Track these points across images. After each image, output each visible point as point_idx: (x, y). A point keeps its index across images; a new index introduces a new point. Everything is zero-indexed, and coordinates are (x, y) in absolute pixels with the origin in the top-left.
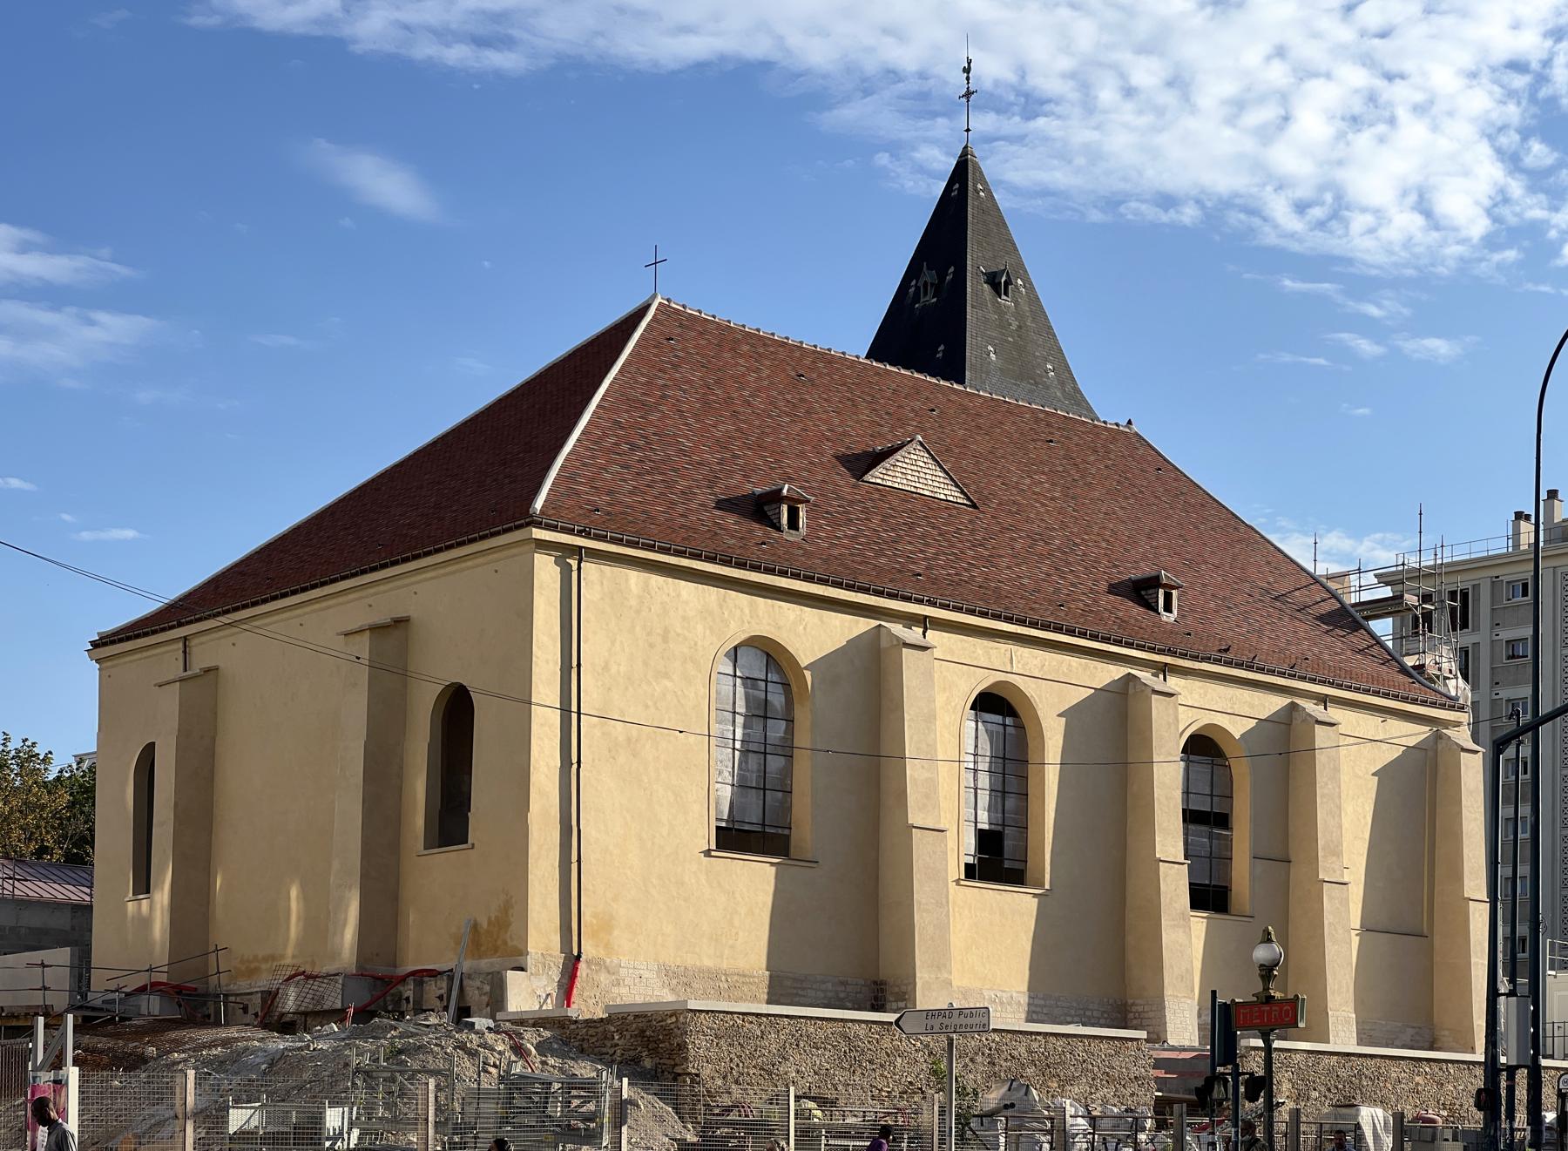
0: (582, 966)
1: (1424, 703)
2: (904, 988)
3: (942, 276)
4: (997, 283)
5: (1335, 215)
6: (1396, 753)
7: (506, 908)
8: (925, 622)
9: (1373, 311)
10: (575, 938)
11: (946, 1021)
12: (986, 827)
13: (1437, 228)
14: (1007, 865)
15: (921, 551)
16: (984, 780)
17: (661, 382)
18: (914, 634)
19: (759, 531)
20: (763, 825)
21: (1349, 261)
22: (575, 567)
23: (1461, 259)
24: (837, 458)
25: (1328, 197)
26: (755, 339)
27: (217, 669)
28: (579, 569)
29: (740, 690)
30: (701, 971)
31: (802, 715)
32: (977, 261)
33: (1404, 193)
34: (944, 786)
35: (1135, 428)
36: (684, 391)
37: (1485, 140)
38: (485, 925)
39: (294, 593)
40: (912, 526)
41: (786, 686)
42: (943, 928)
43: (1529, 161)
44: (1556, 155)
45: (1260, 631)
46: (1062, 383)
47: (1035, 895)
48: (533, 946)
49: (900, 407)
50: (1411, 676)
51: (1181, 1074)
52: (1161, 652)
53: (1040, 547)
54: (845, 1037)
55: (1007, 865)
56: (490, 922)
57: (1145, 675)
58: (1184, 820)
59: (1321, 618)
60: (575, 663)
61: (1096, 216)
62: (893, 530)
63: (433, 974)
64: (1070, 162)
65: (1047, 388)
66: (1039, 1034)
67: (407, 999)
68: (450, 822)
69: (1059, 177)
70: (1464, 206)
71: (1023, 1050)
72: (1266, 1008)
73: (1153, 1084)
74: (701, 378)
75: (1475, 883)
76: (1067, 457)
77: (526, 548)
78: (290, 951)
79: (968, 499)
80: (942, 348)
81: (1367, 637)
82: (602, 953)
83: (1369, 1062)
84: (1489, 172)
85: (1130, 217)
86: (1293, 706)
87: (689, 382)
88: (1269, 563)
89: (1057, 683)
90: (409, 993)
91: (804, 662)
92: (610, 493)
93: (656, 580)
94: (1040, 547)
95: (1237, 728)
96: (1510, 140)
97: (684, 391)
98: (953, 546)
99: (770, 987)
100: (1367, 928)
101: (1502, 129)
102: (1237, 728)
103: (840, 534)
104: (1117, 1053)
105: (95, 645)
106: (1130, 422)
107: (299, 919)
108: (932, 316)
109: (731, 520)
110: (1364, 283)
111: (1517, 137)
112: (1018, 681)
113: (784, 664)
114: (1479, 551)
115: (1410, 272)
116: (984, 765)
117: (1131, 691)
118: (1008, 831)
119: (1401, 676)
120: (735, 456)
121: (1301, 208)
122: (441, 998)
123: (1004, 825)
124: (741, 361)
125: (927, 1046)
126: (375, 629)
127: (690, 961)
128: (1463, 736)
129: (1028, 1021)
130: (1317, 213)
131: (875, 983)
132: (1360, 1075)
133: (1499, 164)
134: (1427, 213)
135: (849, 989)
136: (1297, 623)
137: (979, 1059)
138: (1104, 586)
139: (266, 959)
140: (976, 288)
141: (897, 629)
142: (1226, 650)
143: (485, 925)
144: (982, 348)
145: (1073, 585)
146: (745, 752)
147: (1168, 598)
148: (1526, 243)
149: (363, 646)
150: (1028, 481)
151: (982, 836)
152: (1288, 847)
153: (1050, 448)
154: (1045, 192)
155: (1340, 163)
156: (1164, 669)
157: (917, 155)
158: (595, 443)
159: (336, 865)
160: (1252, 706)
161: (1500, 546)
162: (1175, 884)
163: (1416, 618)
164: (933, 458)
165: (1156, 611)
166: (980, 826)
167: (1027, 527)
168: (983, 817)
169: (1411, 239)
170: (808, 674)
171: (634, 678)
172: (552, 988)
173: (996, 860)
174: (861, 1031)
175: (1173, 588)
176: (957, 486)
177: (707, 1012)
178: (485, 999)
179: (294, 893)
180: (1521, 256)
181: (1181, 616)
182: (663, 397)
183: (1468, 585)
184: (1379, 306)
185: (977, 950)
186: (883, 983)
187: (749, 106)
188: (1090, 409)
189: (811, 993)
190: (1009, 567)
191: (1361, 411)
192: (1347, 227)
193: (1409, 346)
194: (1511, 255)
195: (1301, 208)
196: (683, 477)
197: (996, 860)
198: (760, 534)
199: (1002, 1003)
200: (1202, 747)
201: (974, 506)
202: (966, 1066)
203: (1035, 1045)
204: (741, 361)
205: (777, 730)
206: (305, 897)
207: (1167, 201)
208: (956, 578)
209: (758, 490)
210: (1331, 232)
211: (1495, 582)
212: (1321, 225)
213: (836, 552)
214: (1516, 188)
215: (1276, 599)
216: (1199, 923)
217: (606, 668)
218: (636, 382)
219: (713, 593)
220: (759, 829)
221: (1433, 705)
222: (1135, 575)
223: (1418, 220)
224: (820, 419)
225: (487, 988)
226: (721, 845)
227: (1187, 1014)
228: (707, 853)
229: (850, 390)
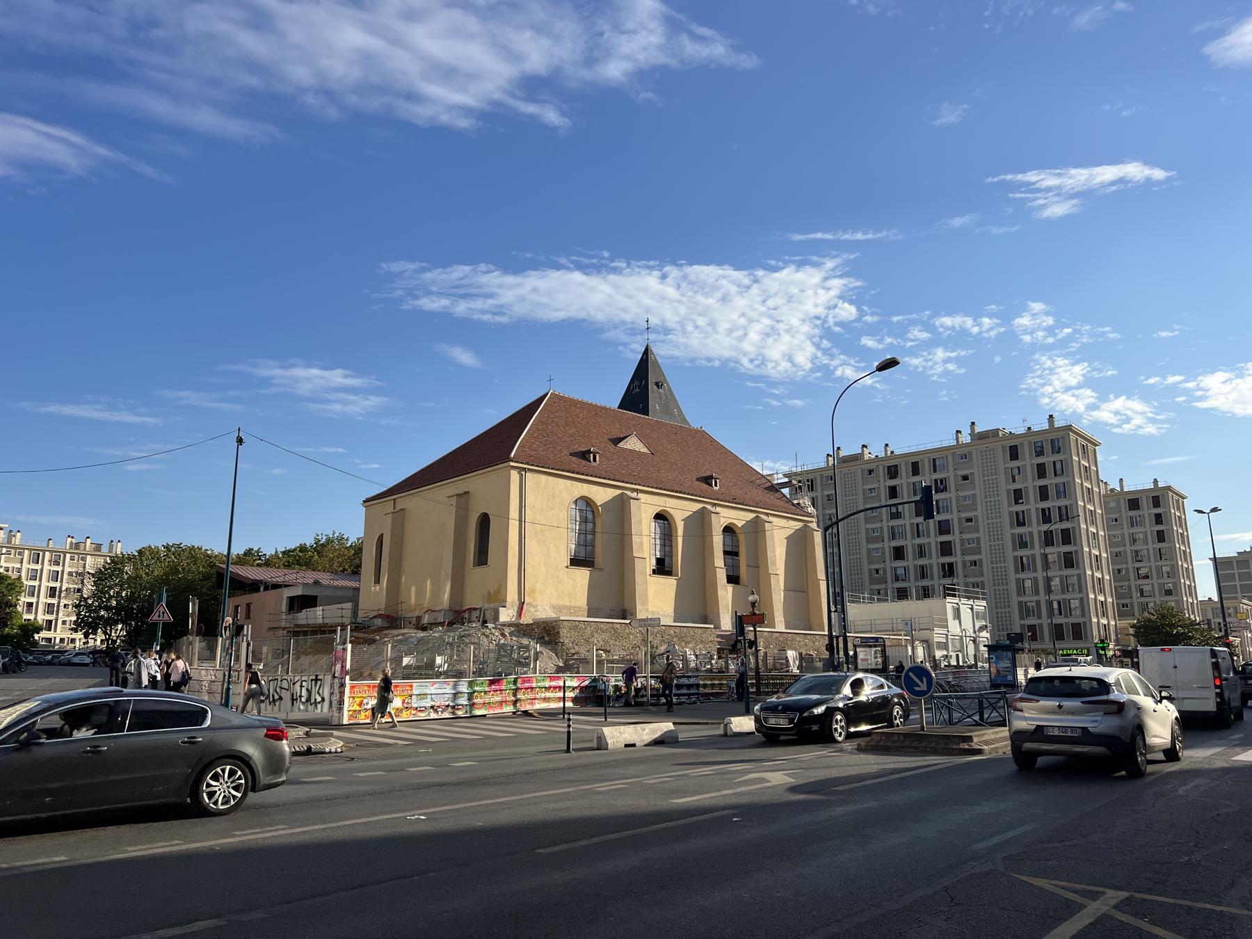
7: (500, 586)
16: (658, 542)
18: (634, 495)
19: (584, 462)
32: (652, 379)
42: (646, 591)
48: (509, 599)
57: (709, 507)
61: (688, 364)
68: (482, 557)
69: (676, 353)
70: (803, 359)
84: (810, 349)
89: (681, 510)
95: (740, 524)
96: (816, 340)
100: (786, 589)
102: (740, 524)
110: (773, 384)
112: (735, 522)
121: (751, 361)
128: (814, 526)
140: (651, 386)
141: (628, 493)
144: (654, 404)
151: (658, 560)
162: (721, 575)
171: (542, 511)
173: (663, 568)
197: (663, 568)
206: (432, 583)
207: (710, 360)
212: (758, 366)
214: (819, 354)
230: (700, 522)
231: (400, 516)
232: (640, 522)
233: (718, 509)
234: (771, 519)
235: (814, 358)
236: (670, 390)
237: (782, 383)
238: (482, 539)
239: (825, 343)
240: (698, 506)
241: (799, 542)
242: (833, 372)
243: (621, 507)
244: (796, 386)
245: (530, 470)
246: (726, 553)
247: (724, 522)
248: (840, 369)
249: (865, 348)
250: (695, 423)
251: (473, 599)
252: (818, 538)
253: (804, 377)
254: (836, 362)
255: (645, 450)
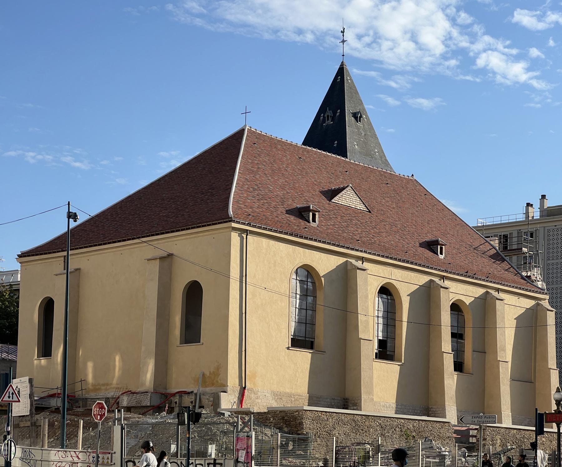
0: (246, 391)
1: (533, 291)
2: (356, 401)
3: (335, 113)
4: (357, 117)
5: (374, 42)
6: (523, 311)
7: (218, 368)
8: (363, 259)
9: (393, 84)
10: (244, 380)
11: (480, 420)
12: (381, 338)
13: (421, 49)
14: (388, 353)
15: (357, 231)
16: (381, 320)
17: (256, 162)
18: (359, 264)
19: (303, 223)
20: (306, 337)
21: (381, 62)
22: (245, 237)
23: (432, 63)
24: (320, 192)
25: (371, 33)
26: (280, 142)
27: (79, 269)
28: (247, 238)
29: (298, 284)
30: (285, 393)
31: (320, 295)
32: (349, 108)
33: (405, 32)
34: (370, 325)
35: (415, 177)
36: (264, 165)
37: (440, 10)
38: (208, 374)
39: (119, 241)
40: (351, 220)
41: (313, 283)
42: (371, 378)
43: (459, 21)
44: (472, 18)
45: (472, 262)
46: (381, 157)
47: (399, 365)
48: (229, 383)
49: (335, 170)
50: (526, 280)
51: (462, 436)
52: (442, 271)
53: (394, 228)
54: (354, 420)
55: (388, 353)
56: (210, 373)
57: (436, 280)
58: (452, 337)
59: (490, 257)
60: (244, 275)
61: (267, 36)
62: (346, 222)
63: (188, 393)
64: (255, 12)
65: (376, 159)
66: (417, 420)
67: (176, 403)
68: (191, 333)
69: (251, 19)
70: (433, 38)
71: (411, 426)
72: (558, 415)
73: (454, 439)
74: (269, 160)
75: (552, 362)
76: (394, 190)
77: (228, 230)
78: (115, 382)
79: (368, 209)
80: (336, 142)
81: (508, 264)
82: (252, 386)
83: (527, 432)
84: (443, 24)
85: (283, 37)
86: (487, 292)
87: (265, 161)
88: (469, 234)
89: (407, 283)
90: (177, 400)
91: (322, 274)
92: (251, 208)
93: (272, 242)
94: (394, 228)
95: (468, 301)
96: (452, 11)
97: (264, 165)
98: (366, 228)
99: (309, 400)
100: (513, 379)
101: (448, 6)
102: (468, 301)
103: (329, 224)
104: (442, 427)
105: (20, 256)
106: (413, 175)
107: (119, 369)
108: (331, 128)
109: (292, 218)
110: (389, 74)
111: (454, 10)
112: (394, 282)
113: (314, 275)
114: (512, 219)
115: (409, 68)
116: (381, 314)
117: (432, 286)
118: (389, 340)
119: (522, 280)
120: (287, 193)
121: (359, 37)
122: (192, 402)
123: (387, 338)
124: (279, 152)
125: (380, 424)
126: (162, 258)
127: (282, 390)
128: (546, 304)
129: (395, 413)
130: (367, 39)
131: (344, 399)
132: (524, 437)
133: (447, 22)
134: (416, 42)
135: (335, 401)
136: (484, 259)
137: (397, 429)
138: (418, 245)
139: (103, 385)
140: (349, 119)
141: (353, 261)
142: (467, 272)
143: (208, 374)
144: (352, 142)
145: (408, 244)
146: (300, 309)
147: (314, 216)
148: (460, 57)
149: (156, 266)
150: (384, 201)
151: (380, 341)
152: (486, 347)
153: (388, 187)
154: (245, 25)
155: (376, 18)
156: (443, 278)
157: (186, 6)
158: (242, 188)
159: (143, 348)
160: (473, 292)
161: (521, 217)
162: (449, 361)
163: (525, 258)
164: (356, 193)
165: (437, 254)
166: (379, 338)
167: (388, 220)
168: (380, 334)
169: (409, 54)
170: (323, 279)
171: (262, 278)
172: (236, 400)
173: (385, 351)
174: (359, 418)
175: (443, 245)
176: (364, 204)
177: (310, 411)
178: (211, 403)
179: (117, 358)
180: (458, 63)
181: (446, 256)
182: (258, 168)
183: (508, 233)
184: (396, 83)
185: (381, 386)
186: (347, 399)
187: (277, 50)
188: (391, 168)
189: (323, 403)
190: (386, 237)
191: (390, 130)
192: (380, 46)
193: (410, 101)
194: (453, 62)
195: (359, 37)
196: (273, 201)
197: (385, 351)
198: (303, 224)
199: (387, 407)
200: (456, 308)
201: (370, 212)
202: (393, 432)
203: (415, 424)
204: (279, 152)
205: (310, 299)
206: (123, 359)
207: (300, 32)
208: (370, 241)
209: (298, 206)
210: (373, 49)
211: (519, 232)
212: (369, 45)
213: (329, 231)
214: (455, 33)
215: (474, 249)
216: (455, 375)
217: (255, 276)
218: (248, 162)
219: (290, 247)
220: (303, 339)
221: (536, 292)
222: (427, 239)
223: (411, 46)
224: (311, 176)
225: (212, 399)
226: (293, 345)
227: (453, 412)
228: (288, 348)
229: (317, 164)
230: (427, 296)
231: (73, 279)
232: (367, 297)
233: (447, 283)
234: (366, 265)
235: (448, 38)
236: (370, 124)
237: (402, 73)
238: (192, 310)
239: (464, 17)
240: (424, 279)
241: (530, 323)
242: (473, 61)
243: (345, 277)
244: (427, 81)
245: (252, 233)
246: (453, 335)
247: (453, 298)
248: (484, 55)
249: (518, 27)
250: (400, 166)
251: (181, 381)
252: (551, 318)
253: (433, 65)
254: (478, 46)
255: (361, 207)
